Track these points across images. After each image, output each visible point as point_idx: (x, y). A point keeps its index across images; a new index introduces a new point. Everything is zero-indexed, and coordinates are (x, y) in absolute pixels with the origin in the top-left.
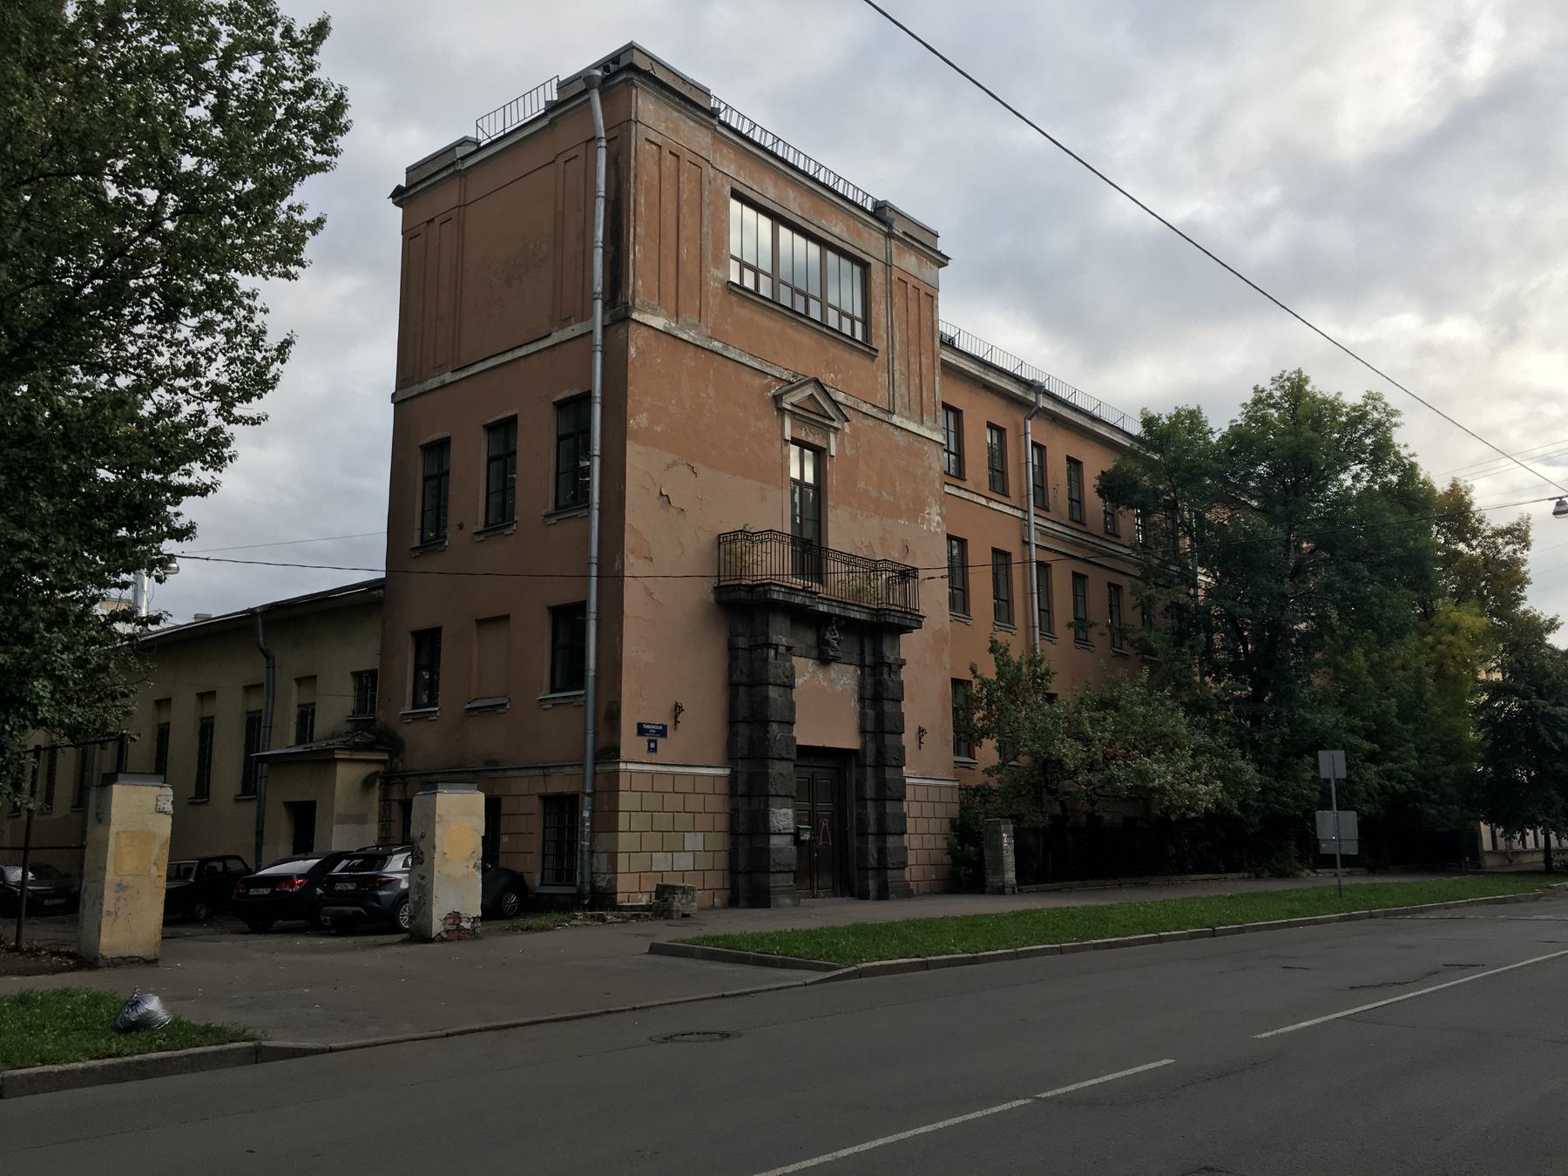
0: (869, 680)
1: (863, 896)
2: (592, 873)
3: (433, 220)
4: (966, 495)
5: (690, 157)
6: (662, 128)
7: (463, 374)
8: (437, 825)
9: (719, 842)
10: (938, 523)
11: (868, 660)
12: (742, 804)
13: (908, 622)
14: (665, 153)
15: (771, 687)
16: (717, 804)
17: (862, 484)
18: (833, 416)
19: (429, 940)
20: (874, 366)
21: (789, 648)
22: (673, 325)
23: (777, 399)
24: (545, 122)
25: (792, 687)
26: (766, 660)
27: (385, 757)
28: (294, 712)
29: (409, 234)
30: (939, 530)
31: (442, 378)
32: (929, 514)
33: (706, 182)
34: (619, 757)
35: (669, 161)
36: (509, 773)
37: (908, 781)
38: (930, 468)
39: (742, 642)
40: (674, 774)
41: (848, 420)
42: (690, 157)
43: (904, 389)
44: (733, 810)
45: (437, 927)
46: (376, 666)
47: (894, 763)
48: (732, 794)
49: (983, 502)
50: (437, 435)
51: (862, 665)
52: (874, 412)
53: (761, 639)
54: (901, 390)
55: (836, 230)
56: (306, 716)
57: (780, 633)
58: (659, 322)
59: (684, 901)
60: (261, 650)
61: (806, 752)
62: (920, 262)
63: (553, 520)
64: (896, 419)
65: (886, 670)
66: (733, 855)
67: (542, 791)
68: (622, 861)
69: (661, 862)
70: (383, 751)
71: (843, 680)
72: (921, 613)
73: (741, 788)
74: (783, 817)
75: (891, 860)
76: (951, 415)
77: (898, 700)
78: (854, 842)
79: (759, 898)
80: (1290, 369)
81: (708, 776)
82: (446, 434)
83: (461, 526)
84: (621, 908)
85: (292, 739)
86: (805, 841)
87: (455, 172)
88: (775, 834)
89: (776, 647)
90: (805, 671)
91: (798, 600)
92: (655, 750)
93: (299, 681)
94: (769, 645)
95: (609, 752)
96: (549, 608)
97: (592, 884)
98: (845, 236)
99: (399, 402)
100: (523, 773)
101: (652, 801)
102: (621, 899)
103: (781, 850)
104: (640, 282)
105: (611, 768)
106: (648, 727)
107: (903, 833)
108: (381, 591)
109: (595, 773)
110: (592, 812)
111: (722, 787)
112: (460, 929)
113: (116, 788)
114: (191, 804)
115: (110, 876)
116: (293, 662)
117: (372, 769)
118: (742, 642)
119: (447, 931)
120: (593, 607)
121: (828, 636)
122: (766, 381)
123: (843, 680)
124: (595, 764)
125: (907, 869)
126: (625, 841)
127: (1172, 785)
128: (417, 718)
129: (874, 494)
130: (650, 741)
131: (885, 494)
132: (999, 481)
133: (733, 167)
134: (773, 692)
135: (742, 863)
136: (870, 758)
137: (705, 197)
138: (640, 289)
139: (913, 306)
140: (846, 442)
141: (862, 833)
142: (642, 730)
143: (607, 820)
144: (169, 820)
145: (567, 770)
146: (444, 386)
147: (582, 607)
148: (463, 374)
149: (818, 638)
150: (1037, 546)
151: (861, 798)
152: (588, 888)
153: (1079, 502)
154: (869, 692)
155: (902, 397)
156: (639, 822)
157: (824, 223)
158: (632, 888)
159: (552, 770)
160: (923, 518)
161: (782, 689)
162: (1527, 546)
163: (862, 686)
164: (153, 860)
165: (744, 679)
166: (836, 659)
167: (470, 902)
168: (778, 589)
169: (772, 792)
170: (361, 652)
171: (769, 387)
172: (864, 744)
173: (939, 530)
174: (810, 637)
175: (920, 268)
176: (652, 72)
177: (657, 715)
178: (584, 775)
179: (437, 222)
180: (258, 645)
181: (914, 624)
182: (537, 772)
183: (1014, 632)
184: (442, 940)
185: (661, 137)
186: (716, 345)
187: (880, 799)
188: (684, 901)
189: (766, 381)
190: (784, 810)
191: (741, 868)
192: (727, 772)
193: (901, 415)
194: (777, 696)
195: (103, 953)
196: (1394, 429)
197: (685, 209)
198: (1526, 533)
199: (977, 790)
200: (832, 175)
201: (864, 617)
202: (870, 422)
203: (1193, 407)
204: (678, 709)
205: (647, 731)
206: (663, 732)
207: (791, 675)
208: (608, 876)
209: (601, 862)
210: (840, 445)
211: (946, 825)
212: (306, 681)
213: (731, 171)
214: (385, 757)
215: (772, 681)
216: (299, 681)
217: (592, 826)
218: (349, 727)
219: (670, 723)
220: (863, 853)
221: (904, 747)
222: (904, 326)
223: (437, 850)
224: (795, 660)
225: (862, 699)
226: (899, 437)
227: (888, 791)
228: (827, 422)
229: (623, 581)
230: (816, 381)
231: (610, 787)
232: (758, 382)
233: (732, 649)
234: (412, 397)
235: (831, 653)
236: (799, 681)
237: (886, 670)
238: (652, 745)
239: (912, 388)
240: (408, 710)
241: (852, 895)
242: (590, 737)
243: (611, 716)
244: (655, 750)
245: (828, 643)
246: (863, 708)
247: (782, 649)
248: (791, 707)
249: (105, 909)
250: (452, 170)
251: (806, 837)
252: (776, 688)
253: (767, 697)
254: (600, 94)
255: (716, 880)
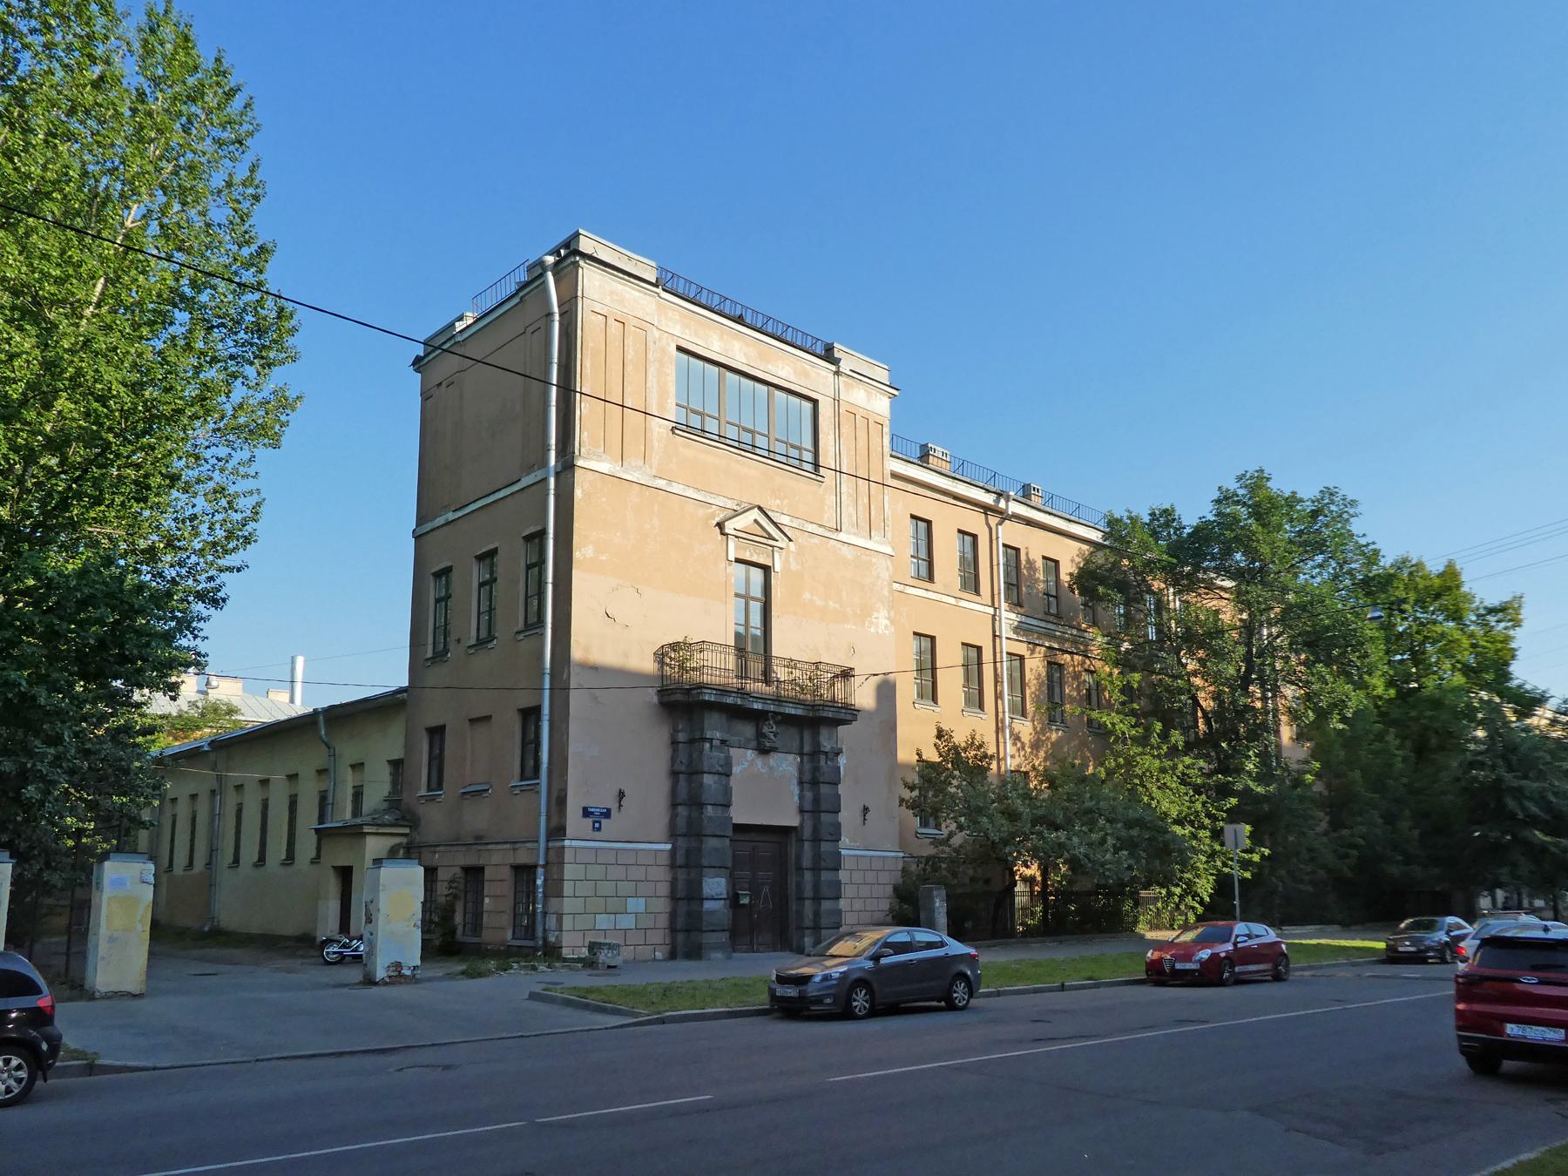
0: (807, 766)
1: (800, 951)
2: (545, 930)
3: (441, 384)
4: (938, 597)
5: (635, 322)
6: (607, 301)
7: (460, 514)
8: (381, 894)
9: (662, 906)
10: (886, 626)
11: (807, 749)
12: (682, 875)
13: (842, 716)
14: (611, 321)
15: (705, 775)
16: (661, 874)
17: (807, 596)
18: (777, 537)
19: (376, 984)
20: (821, 491)
21: (723, 742)
22: (618, 468)
23: (720, 525)
24: (516, 300)
25: (728, 775)
26: (701, 751)
27: (407, 831)
28: (350, 792)
29: (426, 396)
30: (887, 632)
31: (445, 517)
32: (877, 618)
33: (650, 343)
34: (565, 835)
35: (615, 328)
36: (490, 847)
37: (843, 852)
38: (878, 577)
39: (681, 737)
40: (617, 850)
41: (790, 540)
42: (635, 322)
43: (852, 510)
44: (673, 878)
45: (381, 974)
46: (402, 756)
47: (829, 838)
48: (673, 866)
49: (952, 601)
50: (443, 565)
51: (801, 754)
52: (820, 531)
53: (697, 736)
54: (848, 510)
55: (780, 374)
56: (358, 795)
57: (714, 728)
58: (604, 467)
59: (610, 955)
60: (323, 741)
61: (739, 828)
62: (869, 394)
63: (521, 637)
64: (842, 536)
65: (823, 758)
66: (673, 915)
67: (512, 861)
68: (567, 922)
69: (603, 921)
70: (405, 826)
71: (786, 765)
72: (856, 708)
73: (680, 860)
74: (715, 885)
75: (824, 922)
76: (922, 525)
77: (835, 783)
78: (793, 907)
79: (694, 952)
80: (1252, 468)
81: (650, 850)
82: (449, 564)
83: (459, 641)
84: (565, 960)
85: (348, 815)
86: (744, 905)
87: (455, 343)
88: (707, 899)
89: (711, 740)
90: (744, 761)
91: (730, 700)
92: (599, 829)
93: (353, 767)
94: (704, 740)
95: (557, 832)
96: (519, 710)
97: (545, 939)
98: (792, 378)
99: (418, 537)
100: (499, 847)
101: (596, 872)
102: (566, 953)
103: (713, 913)
104: (586, 434)
105: (558, 844)
106: (592, 810)
107: (838, 898)
108: (405, 695)
109: (547, 849)
110: (545, 880)
111: (664, 860)
112: (401, 975)
113: (107, 864)
114: (282, 864)
115: (103, 931)
116: (349, 750)
117: (397, 840)
118: (681, 737)
119: (390, 977)
120: (546, 710)
121: (765, 730)
122: (710, 511)
123: (786, 765)
124: (548, 841)
125: (587, 944)
126: (568, 905)
127: (1086, 856)
128: (432, 799)
129: (819, 603)
130: (594, 822)
131: (831, 603)
132: (971, 583)
133: (678, 327)
134: (708, 779)
135: (680, 923)
136: (807, 833)
137: (650, 356)
138: (586, 440)
139: (862, 435)
140: (791, 560)
141: (801, 899)
142: (586, 813)
143: (555, 888)
144: (152, 887)
145: (528, 845)
146: (448, 523)
147: (537, 710)
148: (460, 514)
149: (757, 731)
150: (1007, 638)
151: (800, 869)
152: (541, 943)
153: (1056, 597)
154: (807, 777)
155: (850, 516)
156: (585, 889)
157: (770, 368)
158: (573, 944)
159: (518, 845)
160: (871, 622)
161: (716, 777)
162: (1517, 623)
163: (801, 771)
164: (139, 918)
165: (683, 768)
166: (774, 750)
167: (412, 955)
168: (709, 691)
169: (705, 862)
170: (386, 744)
171: (713, 516)
172: (803, 821)
173: (887, 632)
174: (748, 730)
175: (869, 401)
176: (595, 255)
177: (599, 802)
178: (538, 849)
179: (444, 384)
180: (321, 737)
181: (849, 717)
182: (508, 846)
183: (984, 717)
184: (386, 984)
185: (606, 308)
186: (661, 483)
187: (816, 869)
188: (610, 955)
189: (710, 511)
190: (717, 879)
191: (679, 926)
192: (669, 847)
193: (849, 533)
194: (712, 783)
195: (100, 988)
196: (1352, 520)
197: (629, 368)
198: (1517, 610)
199: (928, 859)
200: (780, 325)
201: (800, 712)
202: (816, 540)
203: (1167, 506)
204: (621, 795)
205: (592, 813)
206: (607, 814)
207: (728, 763)
208: (556, 933)
209: (552, 922)
210: (786, 562)
211: (889, 889)
212: (357, 767)
213: (677, 330)
214: (407, 831)
215: (706, 769)
216: (353, 767)
217: (544, 892)
218: (385, 805)
219: (614, 806)
220: (800, 914)
221: (840, 824)
222: (853, 453)
223: (381, 912)
224: (733, 751)
225: (801, 783)
226: (845, 549)
227: (823, 863)
228: (771, 542)
229: (568, 693)
230: (760, 508)
231: (556, 861)
232: (702, 512)
233: (674, 743)
234: (428, 532)
235: (768, 745)
236: (736, 770)
237: (823, 758)
238: (597, 825)
239: (860, 508)
240: (423, 792)
241: (791, 951)
242: (543, 819)
243: (559, 802)
244: (599, 829)
245: (764, 736)
246: (802, 790)
247: (716, 743)
248: (727, 791)
249: (99, 955)
250: (453, 342)
251: (745, 901)
252: (711, 776)
253: (701, 784)
254: (554, 275)
255: (659, 937)
